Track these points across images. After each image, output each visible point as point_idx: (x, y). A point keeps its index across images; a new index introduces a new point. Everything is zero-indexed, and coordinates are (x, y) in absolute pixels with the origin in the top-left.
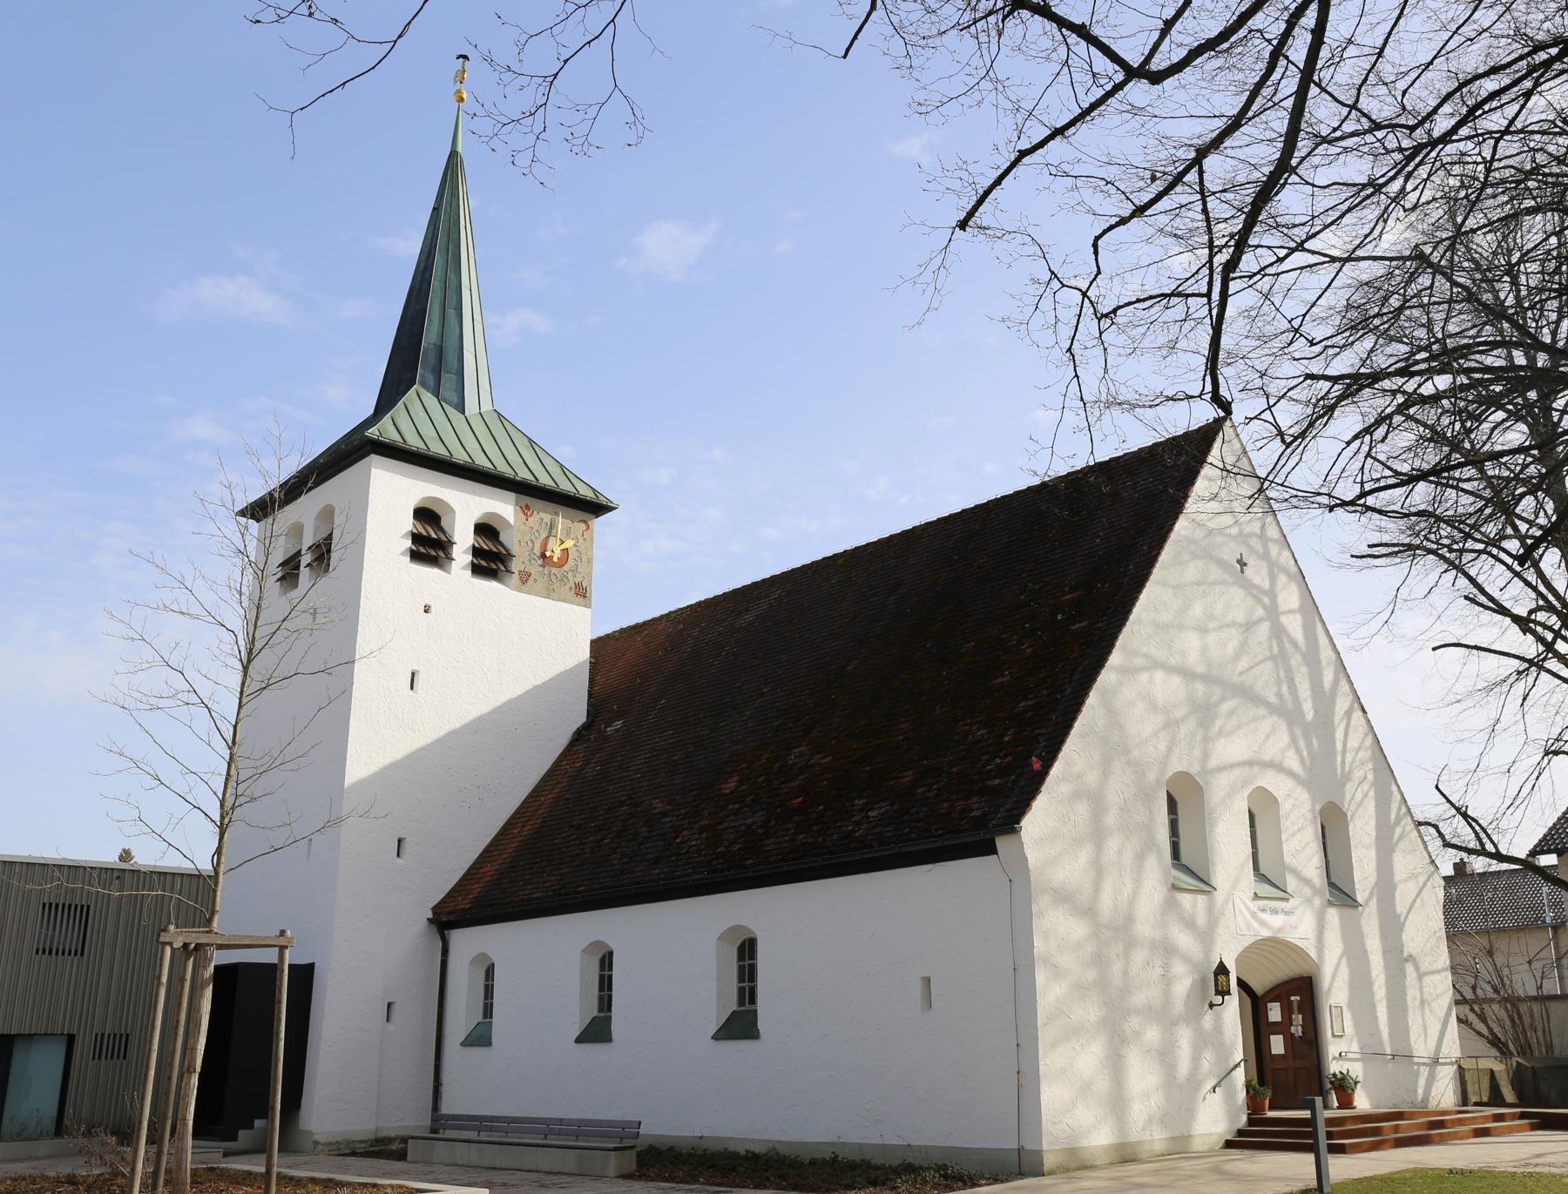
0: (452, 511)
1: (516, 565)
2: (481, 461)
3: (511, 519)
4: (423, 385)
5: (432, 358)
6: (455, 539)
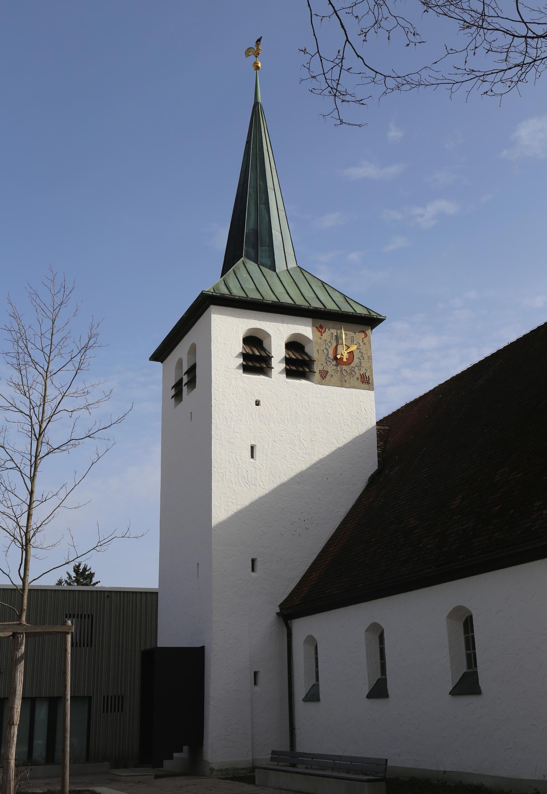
0: (268, 336)
1: (317, 368)
2: (285, 299)
3: (310, 336)
4: (248, 257)
6: (273, 354)
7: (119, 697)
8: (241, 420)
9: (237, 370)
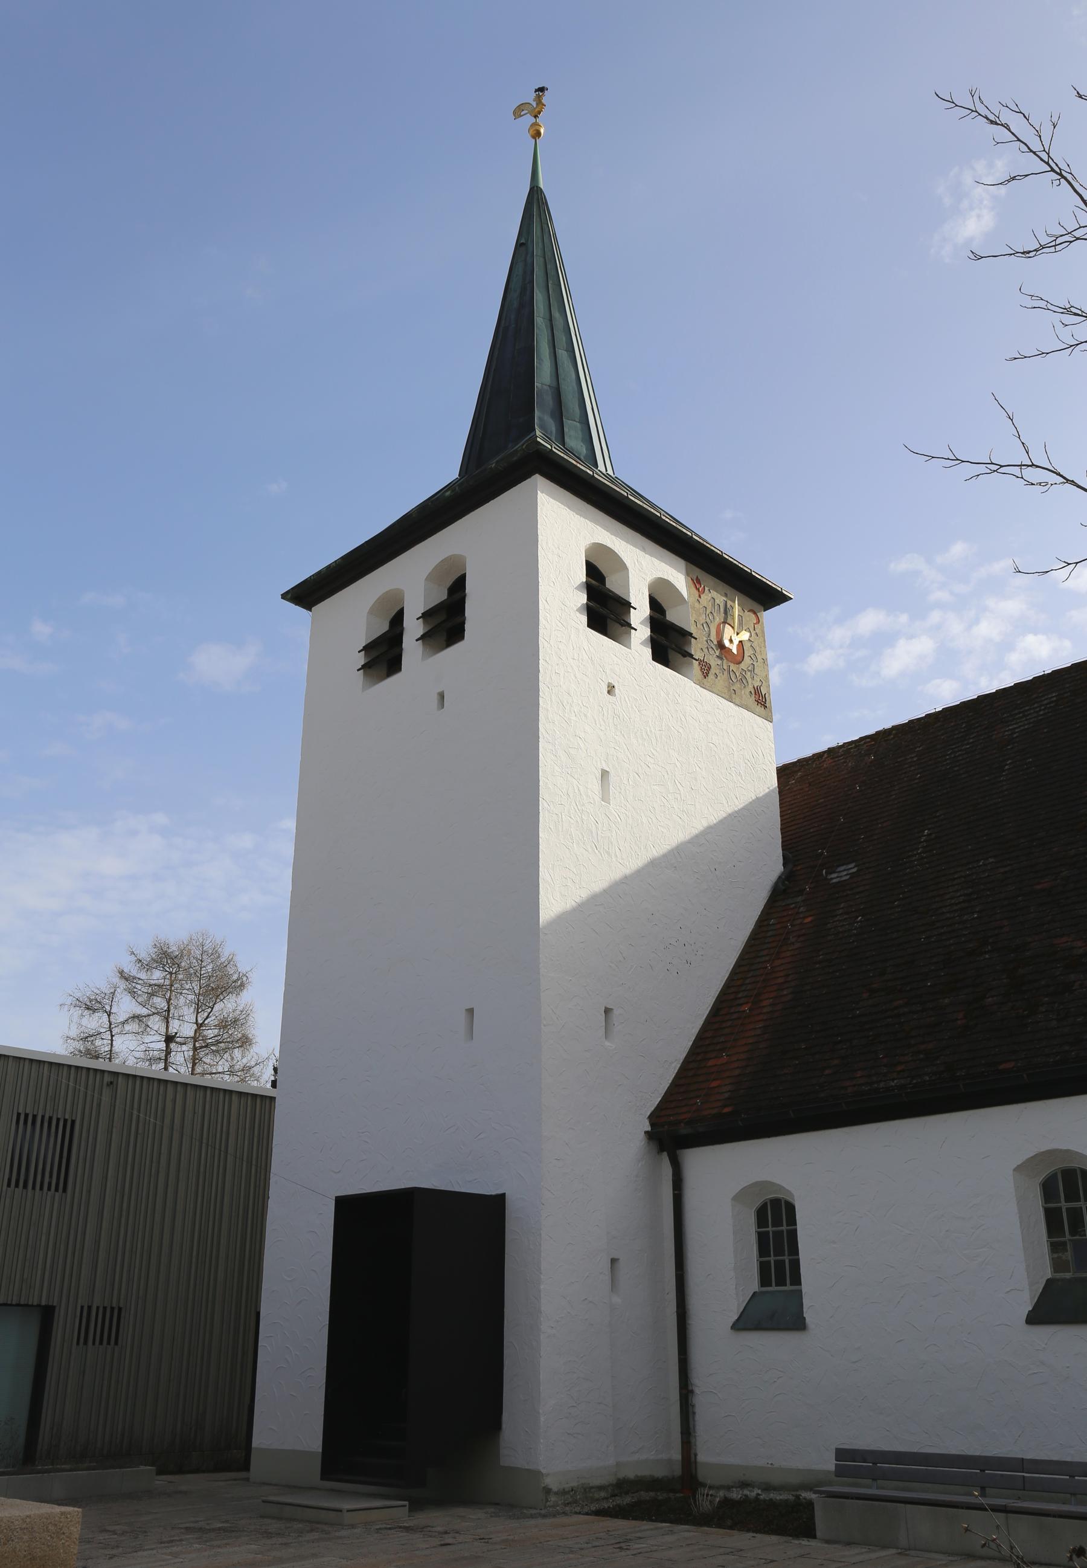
3: (684, 592)
5: (549, 400)
7: (112, 1309)
8: (585, 715)
9: (578, 614)
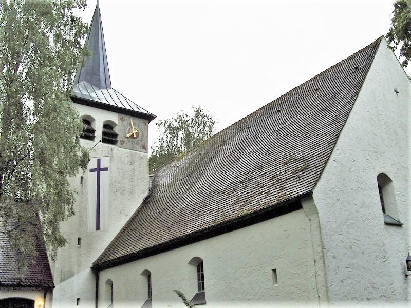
0: (94, 120)
1: (119, 139)
